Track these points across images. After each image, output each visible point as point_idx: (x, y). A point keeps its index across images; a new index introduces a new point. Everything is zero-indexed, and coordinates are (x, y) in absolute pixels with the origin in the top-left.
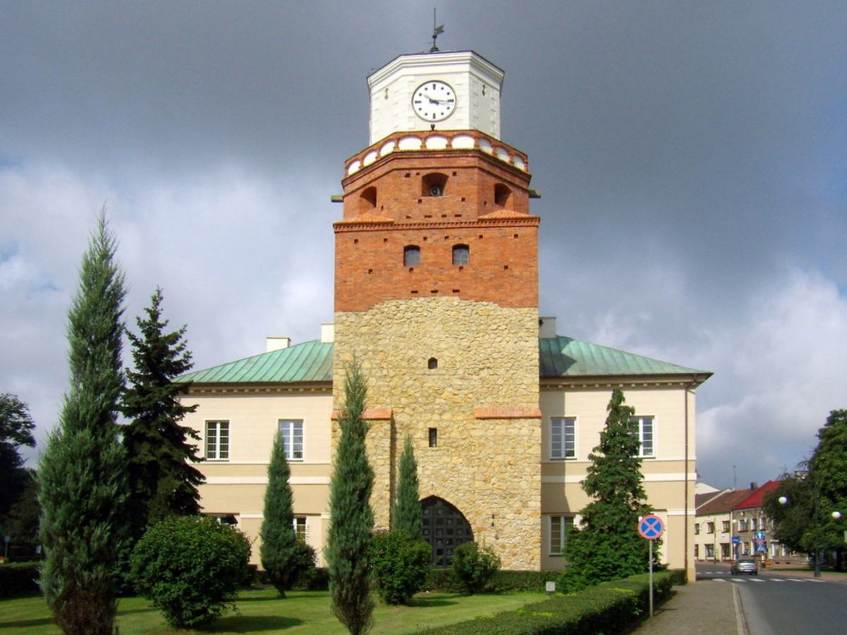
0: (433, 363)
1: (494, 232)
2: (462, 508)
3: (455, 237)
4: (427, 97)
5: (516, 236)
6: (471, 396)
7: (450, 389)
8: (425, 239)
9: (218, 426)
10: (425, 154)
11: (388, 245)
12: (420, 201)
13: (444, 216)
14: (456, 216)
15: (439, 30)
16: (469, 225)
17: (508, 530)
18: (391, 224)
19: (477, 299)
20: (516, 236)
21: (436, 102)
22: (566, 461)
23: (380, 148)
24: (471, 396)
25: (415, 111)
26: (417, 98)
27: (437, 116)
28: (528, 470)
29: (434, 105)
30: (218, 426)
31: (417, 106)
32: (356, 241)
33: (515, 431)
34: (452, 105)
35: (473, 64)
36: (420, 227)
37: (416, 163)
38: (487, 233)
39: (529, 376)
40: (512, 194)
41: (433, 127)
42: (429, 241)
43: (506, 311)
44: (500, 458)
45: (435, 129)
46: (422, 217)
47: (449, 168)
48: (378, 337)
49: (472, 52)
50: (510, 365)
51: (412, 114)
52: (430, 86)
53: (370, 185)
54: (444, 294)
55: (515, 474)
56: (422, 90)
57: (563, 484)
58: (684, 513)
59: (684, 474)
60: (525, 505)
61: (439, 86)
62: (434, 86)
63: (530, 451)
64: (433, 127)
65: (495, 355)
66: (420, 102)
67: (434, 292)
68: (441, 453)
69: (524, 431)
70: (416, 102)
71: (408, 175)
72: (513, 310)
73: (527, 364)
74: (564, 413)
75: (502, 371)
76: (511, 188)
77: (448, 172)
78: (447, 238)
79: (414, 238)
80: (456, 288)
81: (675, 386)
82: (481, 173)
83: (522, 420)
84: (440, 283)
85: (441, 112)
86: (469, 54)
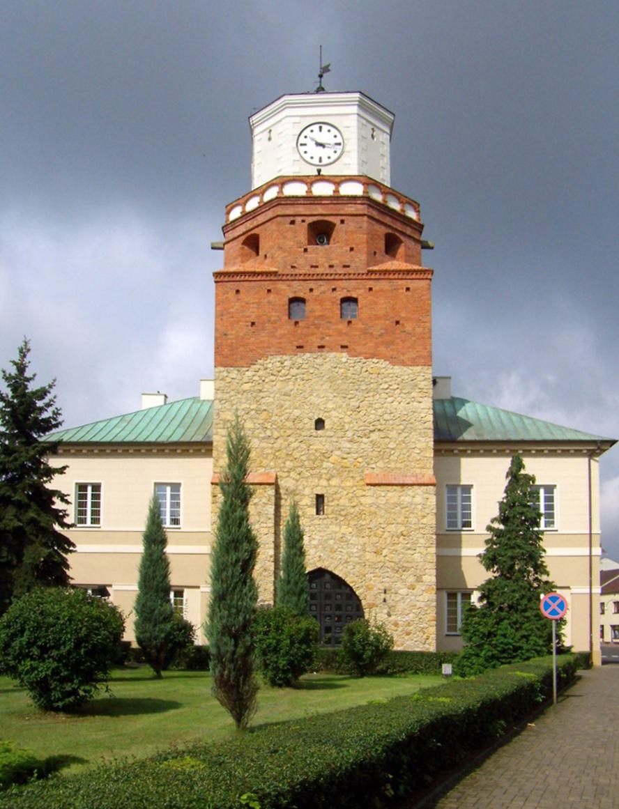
0: (320, 424)
1: (384, 285)
2: (352, 582)
3: (343, 289)
4: (313, 139)
5: (408, 289)
6: (360, 460)
7: (338, 453)
8: (311, 290)
9: (89, 488)
10: (310, 199)
11: (272, 297)
12: (306, 250)
13: (331, 266)
14: (344, 266)
15: (326, 69)
16: (358, 277)
17: (400, 606)
18: (275, 273)
19: (368, 356)
20: (408, 289)
21: (322, 145)
22: (463, 533)
23: (263, 193)
24: (360, 460)
25: (310, 164)
26: (302, 140)
27: (318, 129)
28: (422, 541)
29: (321, 148)
30: (89, 488)
31: (302, 149)
32: (238, 291)
33: (408, 499)
34: (339, 149)
35: (361, 105)
36: (306, 278)
37: (301, 210)
38: (377, 286)
39: (423, 439)
40: (403, 244)
41: (319, 171)
42: (316, 293)
43: (397, 369)
44: (392, 528)
45: (321, 173)
46: (308, 268)
47: (337, 215)
48: (261, 394)
49: (360, 92)
50: (402, 427)
51: (298, 157)
52: (316, 128)
53: (253, 232)
54: (332, 350)
55: (409, 546)
56: (307, 132)
57: (459, 558)
58: (588, 591)
59: (588, 549)
60: (419, 579)
61: (325, 128)
62: (321, 128)
63: (425, 521)
64: (319, 171)
65: (386, 417)
66: (305, 145)
67: (321, 347)
68: (329, 521)
69: (418, 499)
70: (301, 145)
71: (293, 222)
72: (405, 368)
73: (421, 427)
74: (460, 480)
75: (393, 434)
76: (402, 238)
77: (336, 220)
78: (334, 290)
79: (299, 289)
80: (345, 343)
81: (578, 453)
82: (371, 221)
83: (416, 487)
84: (327, 338)
85: (328, 133)
86: (358, 95)
